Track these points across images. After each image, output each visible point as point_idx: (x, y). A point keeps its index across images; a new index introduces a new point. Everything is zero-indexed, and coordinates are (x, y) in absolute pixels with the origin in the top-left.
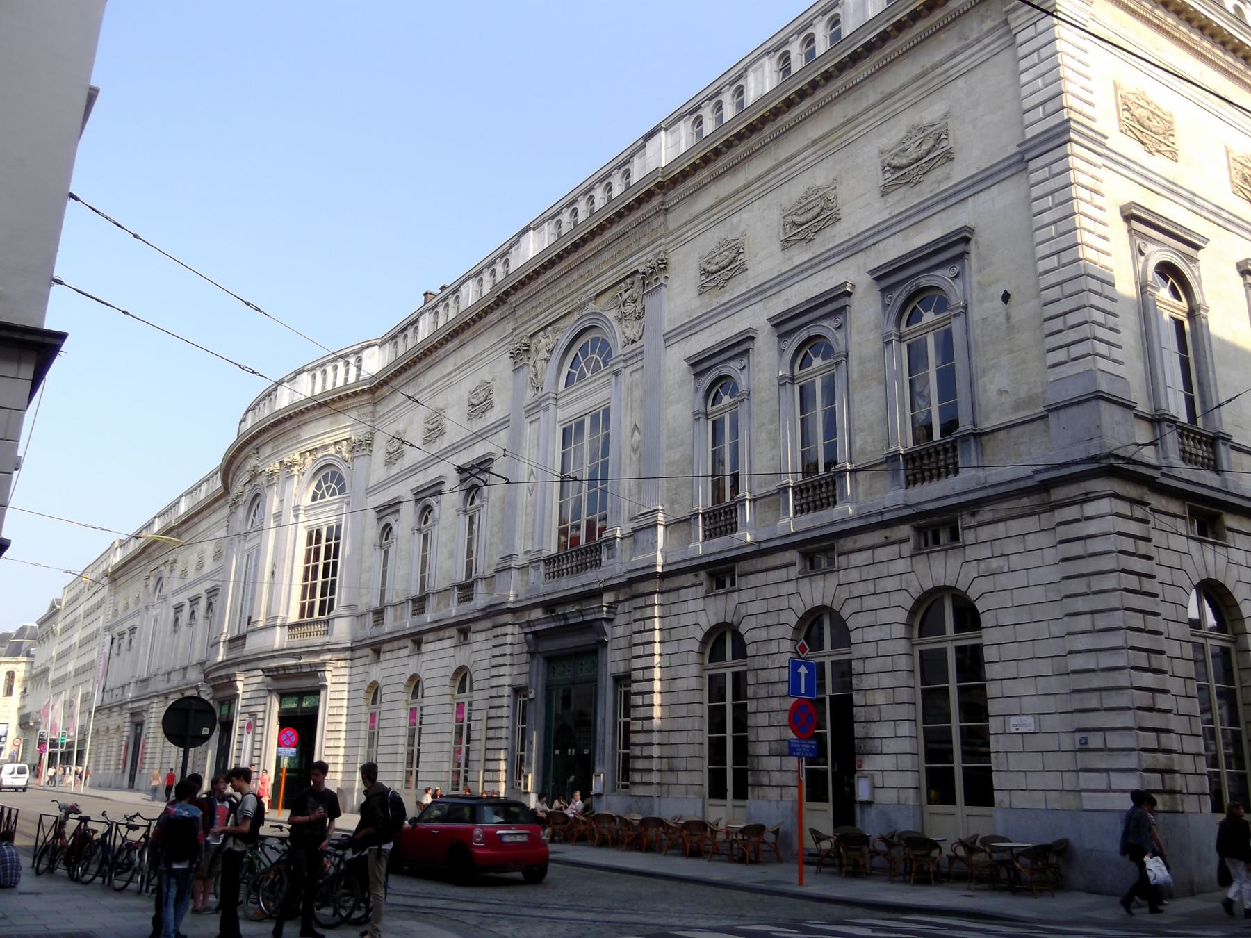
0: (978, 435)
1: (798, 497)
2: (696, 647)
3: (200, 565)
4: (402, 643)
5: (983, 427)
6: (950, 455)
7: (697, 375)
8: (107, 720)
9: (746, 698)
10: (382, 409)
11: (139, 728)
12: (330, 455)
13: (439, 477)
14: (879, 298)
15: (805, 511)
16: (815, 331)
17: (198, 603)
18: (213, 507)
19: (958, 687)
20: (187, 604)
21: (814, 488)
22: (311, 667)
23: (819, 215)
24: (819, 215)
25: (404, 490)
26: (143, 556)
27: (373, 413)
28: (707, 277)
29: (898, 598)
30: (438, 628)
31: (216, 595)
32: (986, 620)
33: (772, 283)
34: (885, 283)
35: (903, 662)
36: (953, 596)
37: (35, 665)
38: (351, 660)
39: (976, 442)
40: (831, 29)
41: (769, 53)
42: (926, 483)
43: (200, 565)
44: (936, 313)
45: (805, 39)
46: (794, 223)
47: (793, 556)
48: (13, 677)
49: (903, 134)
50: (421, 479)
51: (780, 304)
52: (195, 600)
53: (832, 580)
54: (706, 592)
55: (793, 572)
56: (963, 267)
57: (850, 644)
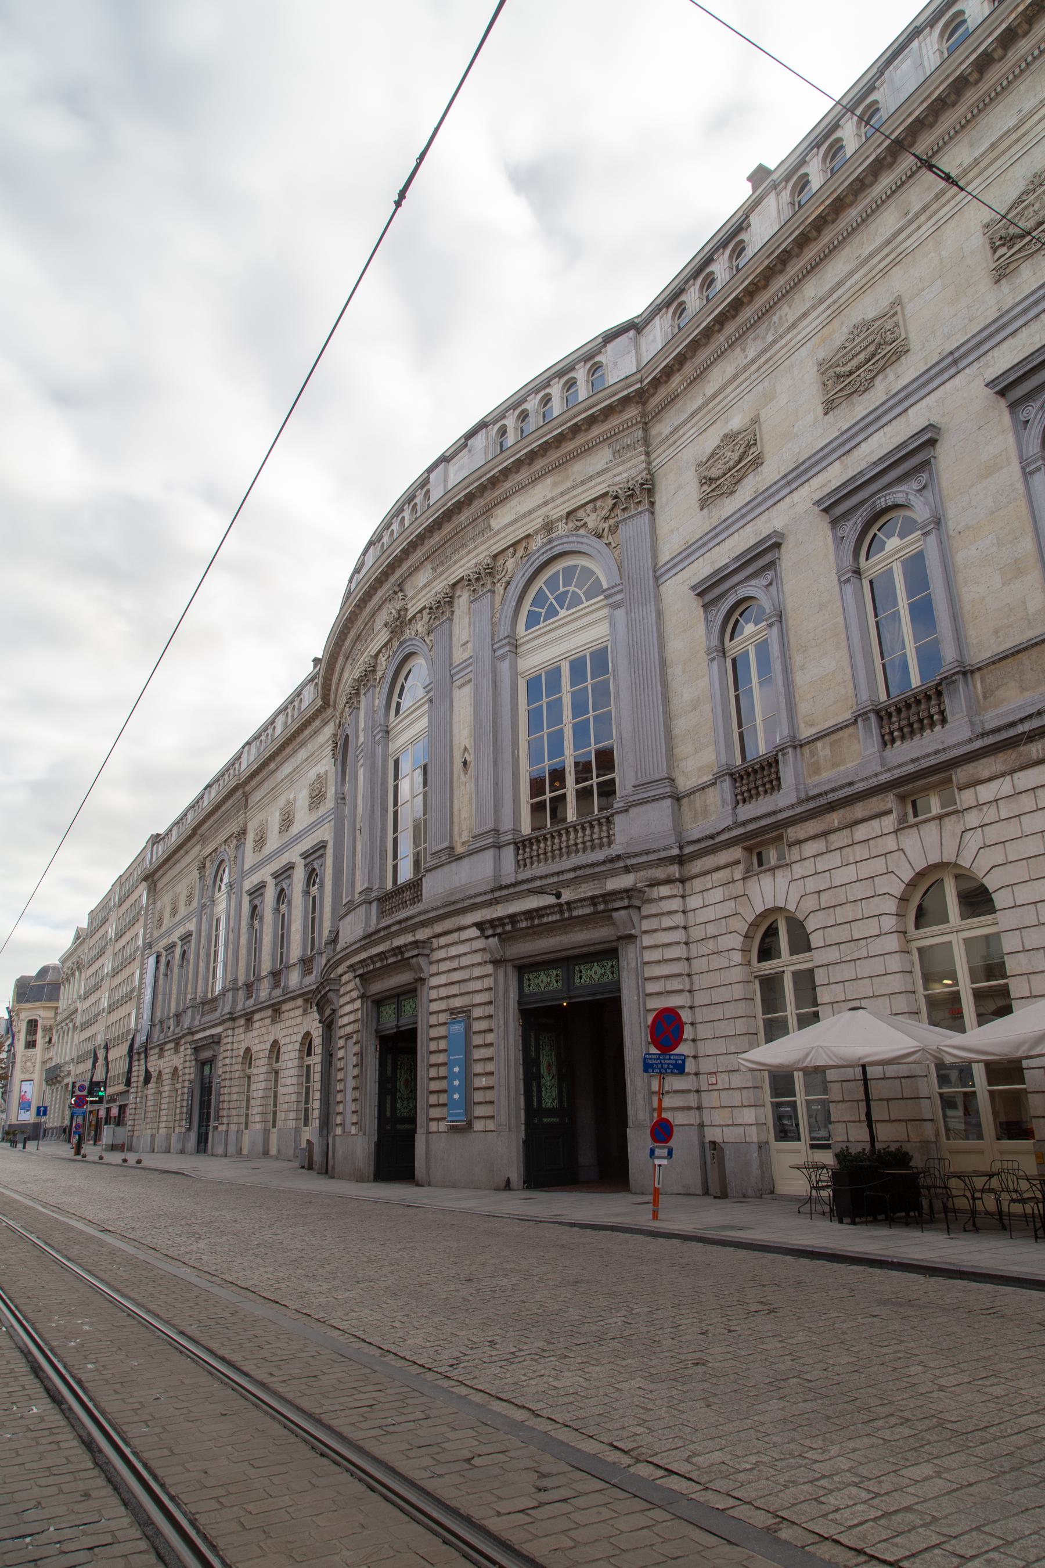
0: (967, 672)
1: (738, 785)
2: (891, 906)
3: (287, 821)
4: (876, 804)
5: (801, 738)
6: (933, 702)
7: (834, 523)
8: (158, 1062)
9: (1007, 977)
10: (662, 429)
11: (207, 1068)
12: (561, 537)
13: (769, 537)
14: (829, 533)
15: (908, 736)
16: (742, 592)
17: (189, 941)
18: (299, 739)
19: (973, 989)
20: (271, 882)
21: (748, 774)
22: (595, 905)
23: (873, 355)
24: (873, 355)
25: (294, 855)
26: (194, 840)
27: (646, 441)
28: (1010, 248)
29: (884, 885)
30: (712, 845)
31: (321, 856)
32: (1000, 900)
33: (857, 428)
34: (708, 598)
35: (895, 963)
36: (957, 877)
37: (60, 1010)
38: (682, 881)
39: (966, 682)
40: (947, 41)
41: (660, 310)
42: (753, 801)
43: (287, 821)
44: (902, 537)
45: (733, 250)
46: (839, 376)
47: (889, 801)
48: (36, 1026)
49: (717, 443)
50: (306, 844)
51: (702, 568)
52: (285, 873)
53: (782, 878)
54: (900, 823)
55: (889, 823)
56: (931, 474)
57: (809, 949)
